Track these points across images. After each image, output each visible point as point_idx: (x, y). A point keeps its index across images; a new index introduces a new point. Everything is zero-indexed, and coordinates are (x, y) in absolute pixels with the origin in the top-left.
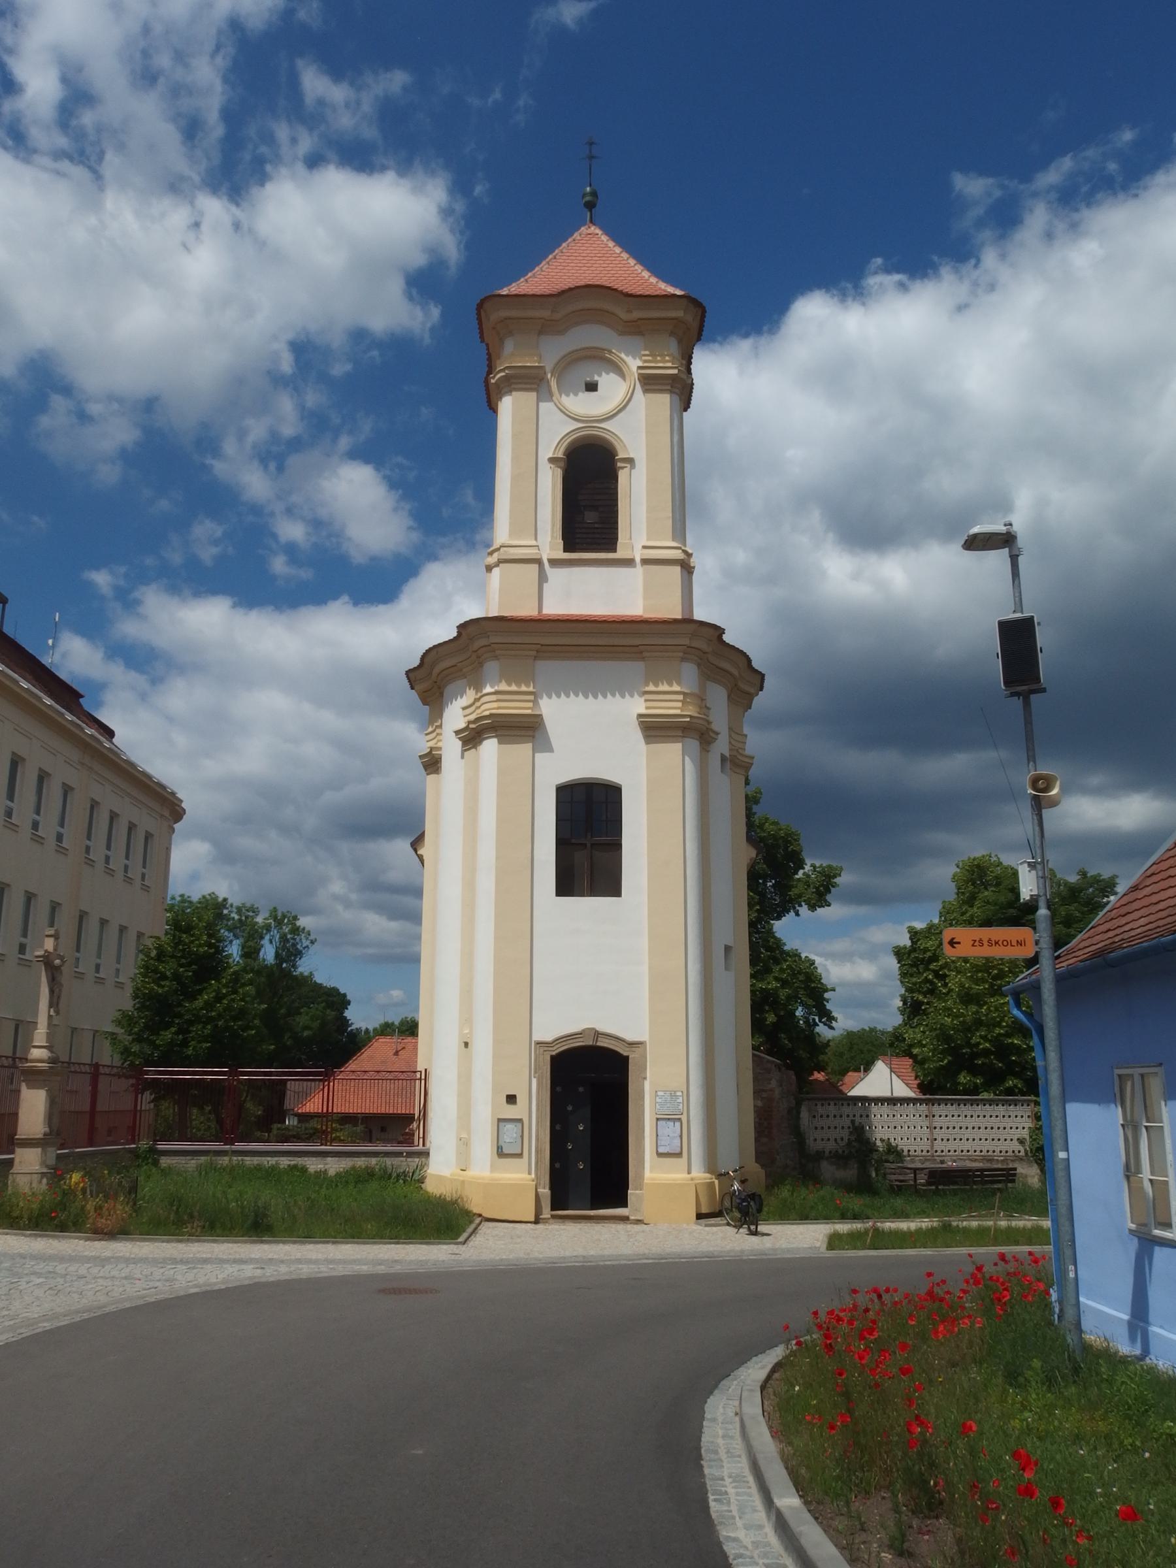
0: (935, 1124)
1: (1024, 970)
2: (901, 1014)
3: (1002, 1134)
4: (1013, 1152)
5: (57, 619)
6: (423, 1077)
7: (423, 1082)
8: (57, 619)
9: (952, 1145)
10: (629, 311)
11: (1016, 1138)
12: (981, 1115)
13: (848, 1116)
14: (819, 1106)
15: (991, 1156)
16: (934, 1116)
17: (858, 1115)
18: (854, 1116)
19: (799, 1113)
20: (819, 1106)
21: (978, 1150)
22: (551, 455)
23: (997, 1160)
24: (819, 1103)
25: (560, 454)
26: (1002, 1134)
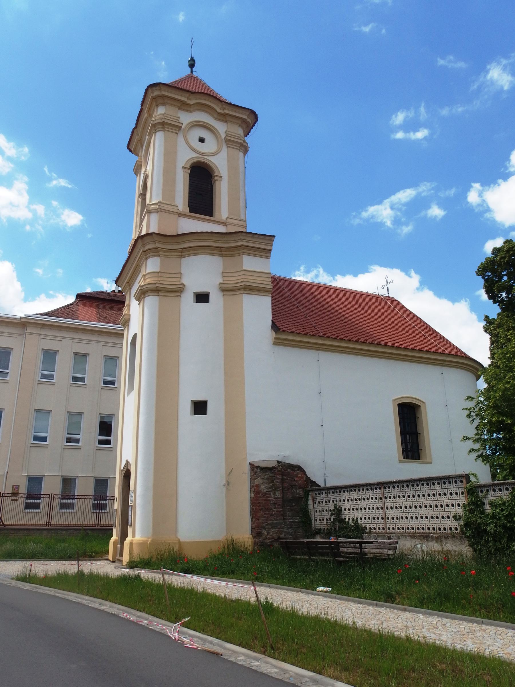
0: (387, 505)
1: (87, 557)
2: (490, 351)
3: (439, 512)
4: (451, 529)
5: (156, 624)
6: (50, 497)
7: (50, 499)
8: (156, 624)
9: (400, 524)
10: (223, 109)
11: (452, 515)
12: (421, 494)
13: (333, 501)
14: (318, 495)
15: (426, 533)
16: (386, 498)
17: (338, 501)
18: (337, 501)
19: (307, 500)
20: (318, 495)
21: (448, 528)
22: (183, 166)
23: (432, 537)
24: (317, 493)
25: (188, 166)
26: (439, 512)
